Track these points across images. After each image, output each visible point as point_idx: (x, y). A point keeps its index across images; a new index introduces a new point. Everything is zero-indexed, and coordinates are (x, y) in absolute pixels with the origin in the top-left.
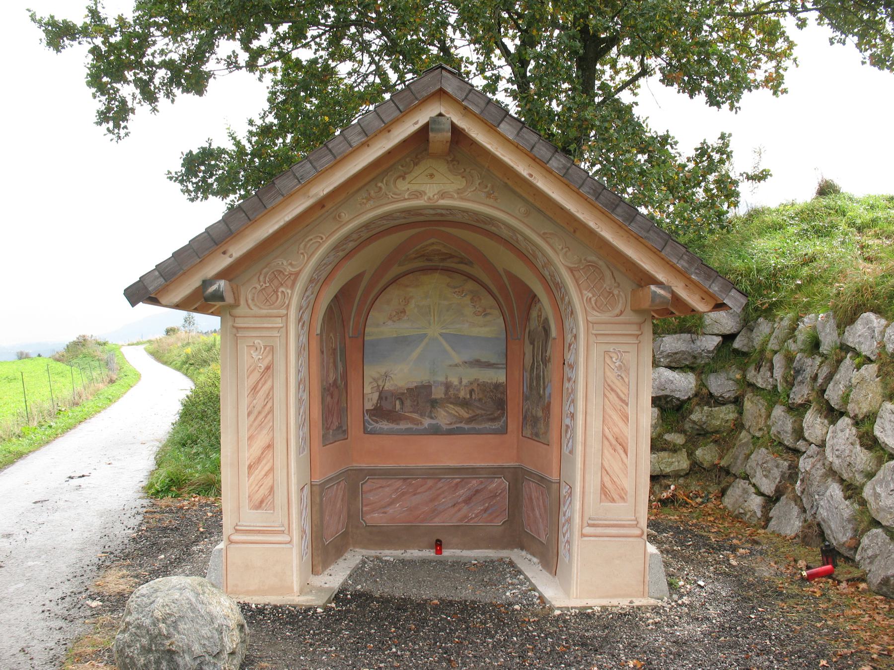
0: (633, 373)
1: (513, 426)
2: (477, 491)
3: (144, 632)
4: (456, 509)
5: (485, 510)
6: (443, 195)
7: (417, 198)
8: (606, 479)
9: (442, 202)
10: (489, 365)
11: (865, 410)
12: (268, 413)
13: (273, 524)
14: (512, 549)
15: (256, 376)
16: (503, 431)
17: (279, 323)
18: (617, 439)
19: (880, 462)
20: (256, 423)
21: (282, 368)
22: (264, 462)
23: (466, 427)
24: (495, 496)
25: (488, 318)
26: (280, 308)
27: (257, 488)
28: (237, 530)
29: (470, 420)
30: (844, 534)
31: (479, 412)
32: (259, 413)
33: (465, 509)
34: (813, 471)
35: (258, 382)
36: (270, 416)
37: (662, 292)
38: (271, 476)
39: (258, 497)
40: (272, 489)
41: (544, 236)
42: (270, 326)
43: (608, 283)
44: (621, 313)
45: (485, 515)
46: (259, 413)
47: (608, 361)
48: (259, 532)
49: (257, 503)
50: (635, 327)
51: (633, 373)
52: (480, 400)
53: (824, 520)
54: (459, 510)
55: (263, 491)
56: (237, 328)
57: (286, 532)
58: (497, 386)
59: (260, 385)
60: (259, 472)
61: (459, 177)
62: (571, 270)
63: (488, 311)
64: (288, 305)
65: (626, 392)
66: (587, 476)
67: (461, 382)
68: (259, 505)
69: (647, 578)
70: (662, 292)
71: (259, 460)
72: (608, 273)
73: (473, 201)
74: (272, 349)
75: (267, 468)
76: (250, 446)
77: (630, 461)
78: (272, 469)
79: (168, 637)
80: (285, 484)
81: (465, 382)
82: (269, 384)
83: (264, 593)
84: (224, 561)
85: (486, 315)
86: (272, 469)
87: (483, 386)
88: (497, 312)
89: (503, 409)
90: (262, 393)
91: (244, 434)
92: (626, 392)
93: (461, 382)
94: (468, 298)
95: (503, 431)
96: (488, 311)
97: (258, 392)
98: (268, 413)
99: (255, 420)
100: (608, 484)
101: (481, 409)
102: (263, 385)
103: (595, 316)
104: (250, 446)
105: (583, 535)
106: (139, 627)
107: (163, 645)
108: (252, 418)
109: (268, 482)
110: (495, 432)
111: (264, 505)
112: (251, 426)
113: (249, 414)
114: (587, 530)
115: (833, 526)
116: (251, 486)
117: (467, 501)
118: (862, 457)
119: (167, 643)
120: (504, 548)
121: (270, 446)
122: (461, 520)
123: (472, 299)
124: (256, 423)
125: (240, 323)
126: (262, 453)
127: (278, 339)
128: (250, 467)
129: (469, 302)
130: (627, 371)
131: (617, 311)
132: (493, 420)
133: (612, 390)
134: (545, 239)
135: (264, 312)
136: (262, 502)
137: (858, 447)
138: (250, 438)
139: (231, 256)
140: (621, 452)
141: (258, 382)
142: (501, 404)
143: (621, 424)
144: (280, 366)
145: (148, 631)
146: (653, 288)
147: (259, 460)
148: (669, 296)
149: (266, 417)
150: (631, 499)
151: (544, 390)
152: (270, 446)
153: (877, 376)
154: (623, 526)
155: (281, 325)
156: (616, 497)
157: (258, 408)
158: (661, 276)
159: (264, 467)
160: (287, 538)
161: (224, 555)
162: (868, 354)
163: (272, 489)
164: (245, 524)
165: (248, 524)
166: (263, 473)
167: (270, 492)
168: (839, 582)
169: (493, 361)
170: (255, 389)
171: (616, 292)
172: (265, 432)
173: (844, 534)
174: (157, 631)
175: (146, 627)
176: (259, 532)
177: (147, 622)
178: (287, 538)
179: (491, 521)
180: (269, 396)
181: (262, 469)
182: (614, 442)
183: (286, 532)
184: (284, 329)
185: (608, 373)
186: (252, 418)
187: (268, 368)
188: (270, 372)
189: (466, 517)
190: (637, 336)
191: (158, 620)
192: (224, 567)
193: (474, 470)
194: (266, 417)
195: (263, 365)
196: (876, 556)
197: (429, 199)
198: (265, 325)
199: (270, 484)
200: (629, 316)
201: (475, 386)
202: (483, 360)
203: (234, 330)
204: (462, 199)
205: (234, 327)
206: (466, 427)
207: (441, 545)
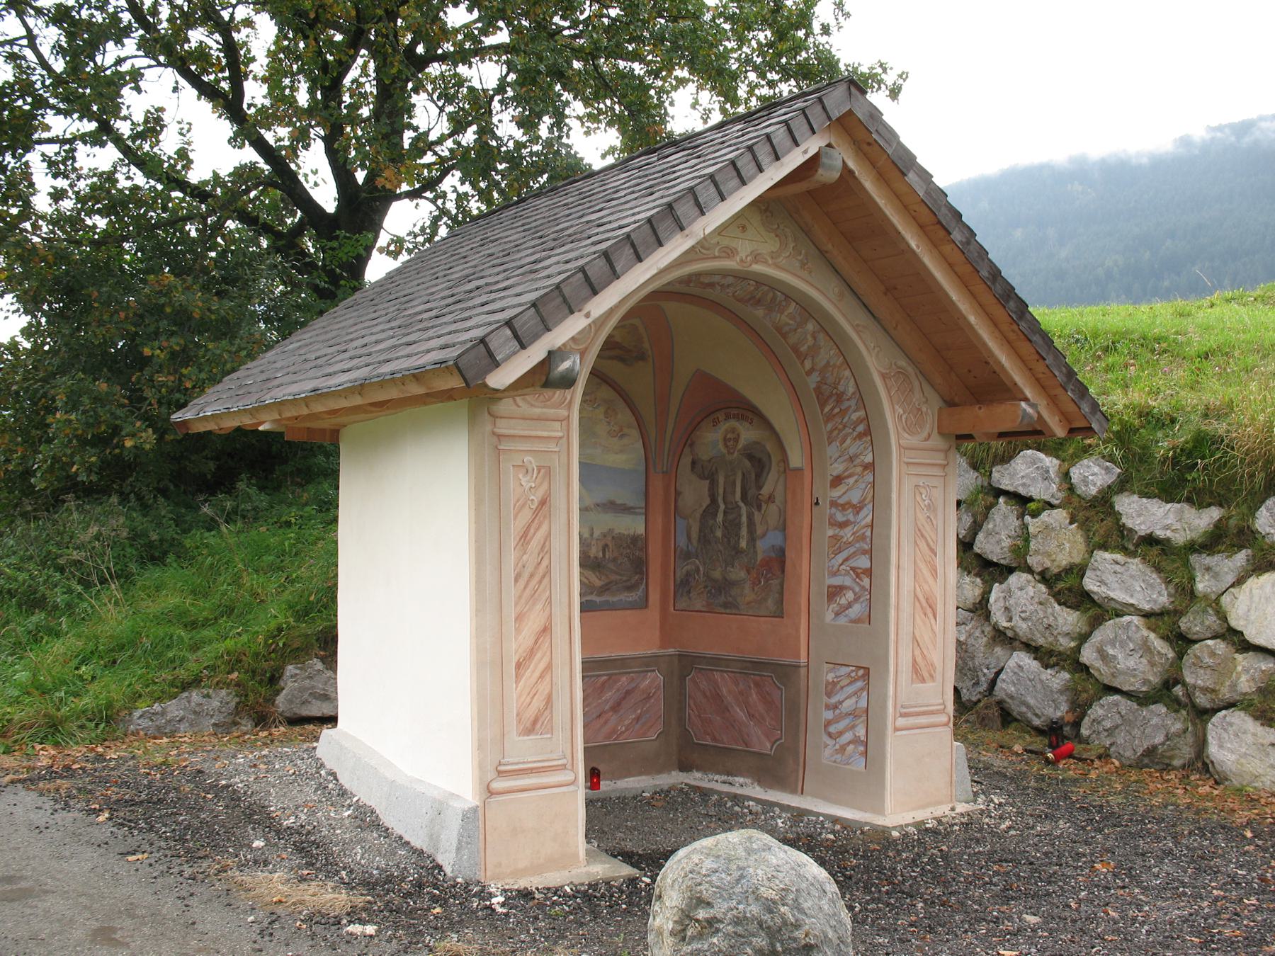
0: (940, 515)
1: (655, 597)
2: (628, 693)
3: (753, 927)
4: (602, 720)
5: (638, 719)
6: (757, 258)
7: (728, 257)
8: (917, 652)
9: (757, 268)
10: (626, 509)
11: (1064, 563)
12: (544, 576)
13: (550, 756)
14: (669, 771)
15: (526, 515)
16: (644, 604)
17: (556, 430)
18: (927, 600)
19: (1096, 622)
20: (528, 592)
21: (563, 506)
22: (539, 655)
23: (598, 599)
24: (649, 698)
25: (626, 441)
26: (559, 406)
27: (528, 700)
28: (500, 773)
29: (604, 589)
30: (1057, 708)
31: (614, 577)
32: (532, 576)
33: (614, 719)
34: (971, 641)
35: (529, 527)
36: (546, 580)
37: (1029, 410)
38: (548, 678)
39: (530, 714)
40: (549, 700)
41: (856, 328)
42: (545, 434)
43: (917, 397)
44: (929, 435)
45: (637, 727)
46: (532, 576)
47: (918, 498)
48: (532, 771)
49: (528, 725)
50: (942, 455)
51: (940, 515)
52: (615, 560)
53: (1012, 697)
54: (605, 723)
55: (538, 703)
56: (499, 436)
57: (569, 766)
58: (635, 539)
59: (532, 531)
60: (532, 673)
61: (773, 235)
62: (884, 376)
63: (626, 430)
64: (570, 402)
65: (934, 537)
66: (900, 651)
67: (592, 535)
68: (530, 729)
69: (954, 778)
70: (1029, 410)
71: (532, 652)
72: (916, 384)
73: (787, 271)
74: (549, 471)
75: (542, 666)
76: (518, 630)
77: (938, 628)
78: (549, 667)
79: (797, 926)
80: (568, 689)
81: (597, 534)
82: (545, 528)
83: (537, 869)
84: (481, 826)
85: (622, 436)
86: (549, 667)
87: (618, 539)
88: (635, 433)
89: (641, 573)
90: (535, 544)
91: (510, 612)
92: (934, 537)
93: (592, 535)
94: (602, 409)
95: (644, 604)
96: (626, 430)
97: (529, 542)
98: (544, 576)
99: (525, 588)
100: (919, 659)
101: (616, 573)
102: (537, 529)
103: (908, 440)
104: (518, 630)
105: (896, 729)
106: (737, 921)
107: (795, 940)
108: (522, 583)
109: (544, 688)
110: (633, 606)
111: (538, 726)
112: (520, 597)
113: (516, 580)
114: (901, 722)
115: (1032, 701)
116: (519, 696)
117: (616, 708)
118: (1068, 619)
119: (799, 934)
120: (660, 772)
121: (546, 630)
122: (608, 737)
123: (606, 412)
124: (528, 592)
125: (504, 427)
126: (536, 642)
127: (556, 457)
128: (518, 666)
129: (602, 416)
130: (935, 510)
131: (925, 434)
132: (630, 588)
133: (922, 536)
134: (858, 332)
135: (537, 411)
136: (535, 722)
137: (1057, 607)
138: (519, 618)
139: (588, 315)
140: (931, 616)
141: (529, 527)
142: (640, 566)
143: (930, 580)
144: (559, 501)
145: (760, 924)
146: (1023, 404)
147: (532, 652)
148: (1035, 416)
149: (540, 582)
150: (938, 677)
151: (752, 540)
152: (546, 630)
153: (1071, 523)
154: (932, 713)
155: (560, 434)
156: (926, 675)
157: (529, 569)
158: (1028, 393)
159: (538, 665)
160: (569, 777)
161: (481, 818)
162: (1046, 497)
163: (549, 700)
164: (511, 760)
165: (516, 760)
166: (537, 674)
167: (547, 703)
168: (1092, 761)
169: (630, 504)
170: (525, 537)
171: (924, 409)
172: (539, 606)
173: (1057, 708)
174: (778, 921)
175: (754, 918)
176: (532, 771)
177: (754, 909)
178: (569, 777)
179: (644, 735)
180: (545, 549)
181: (536, 667)
182: (925, 604)
183: (569, 766)
184: (565, 440)
185: (919, 515)
186: (522, 583)
187: (543, 503)
188: (545, 508)
189: (614, 731)
190: (944, 466)
191: (774, 902)
192: (482, 837)
193: (622, 662)
194: (540, 582)
195: (536, 498)
196: (1117, 727)
197: (742, 260)
198: (540, 433)
199: (547, 692)
200: (937, 442)
201: (609, 540)
202: (619, 502)
203: (495, 439)
204: (777, 266)
205: (494, 433)
206: (598, 599)
207: (598, 775)
